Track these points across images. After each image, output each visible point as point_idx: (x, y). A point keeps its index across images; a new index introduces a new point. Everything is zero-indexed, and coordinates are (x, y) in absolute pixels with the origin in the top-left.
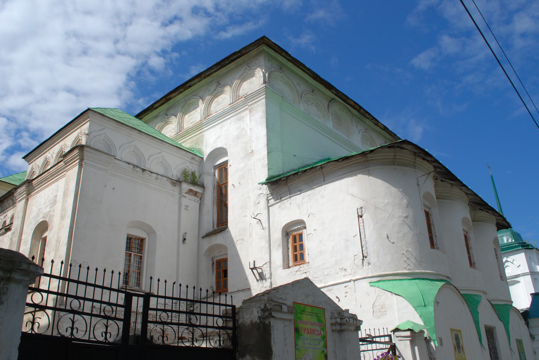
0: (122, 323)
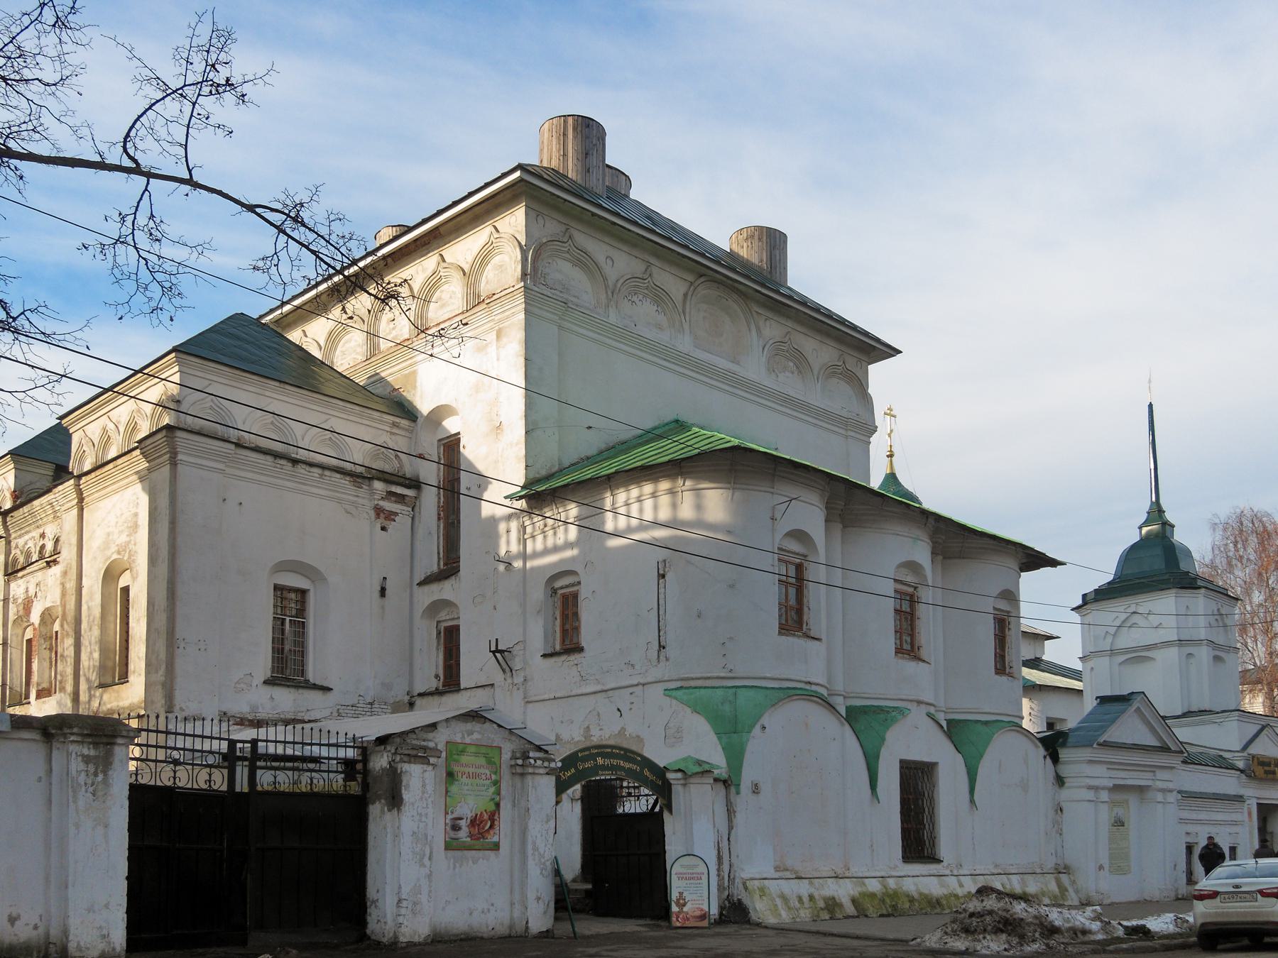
0: (226, 770)
